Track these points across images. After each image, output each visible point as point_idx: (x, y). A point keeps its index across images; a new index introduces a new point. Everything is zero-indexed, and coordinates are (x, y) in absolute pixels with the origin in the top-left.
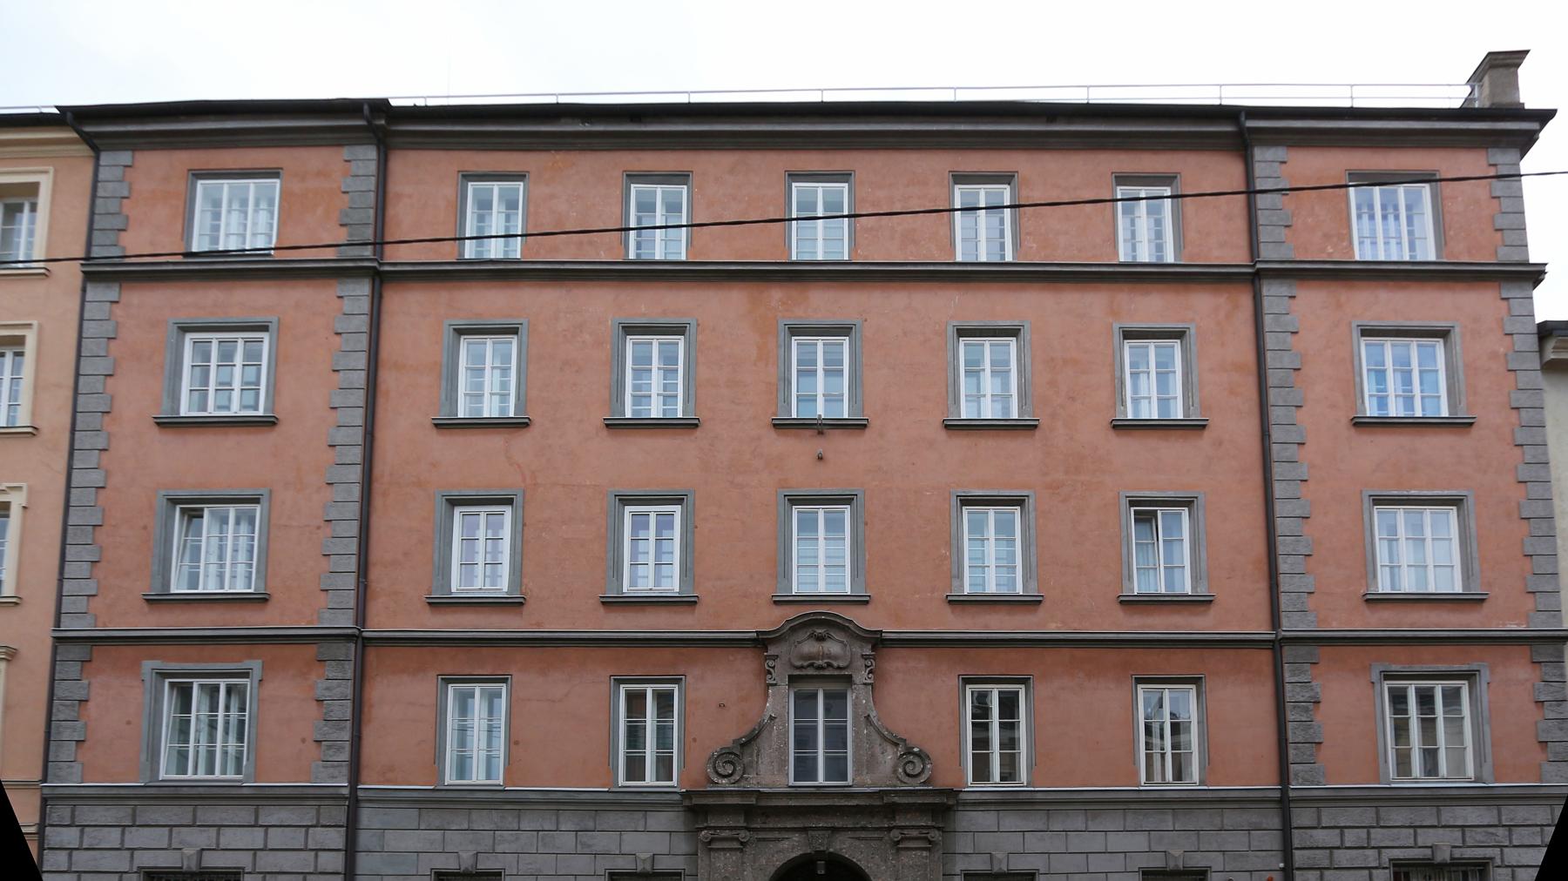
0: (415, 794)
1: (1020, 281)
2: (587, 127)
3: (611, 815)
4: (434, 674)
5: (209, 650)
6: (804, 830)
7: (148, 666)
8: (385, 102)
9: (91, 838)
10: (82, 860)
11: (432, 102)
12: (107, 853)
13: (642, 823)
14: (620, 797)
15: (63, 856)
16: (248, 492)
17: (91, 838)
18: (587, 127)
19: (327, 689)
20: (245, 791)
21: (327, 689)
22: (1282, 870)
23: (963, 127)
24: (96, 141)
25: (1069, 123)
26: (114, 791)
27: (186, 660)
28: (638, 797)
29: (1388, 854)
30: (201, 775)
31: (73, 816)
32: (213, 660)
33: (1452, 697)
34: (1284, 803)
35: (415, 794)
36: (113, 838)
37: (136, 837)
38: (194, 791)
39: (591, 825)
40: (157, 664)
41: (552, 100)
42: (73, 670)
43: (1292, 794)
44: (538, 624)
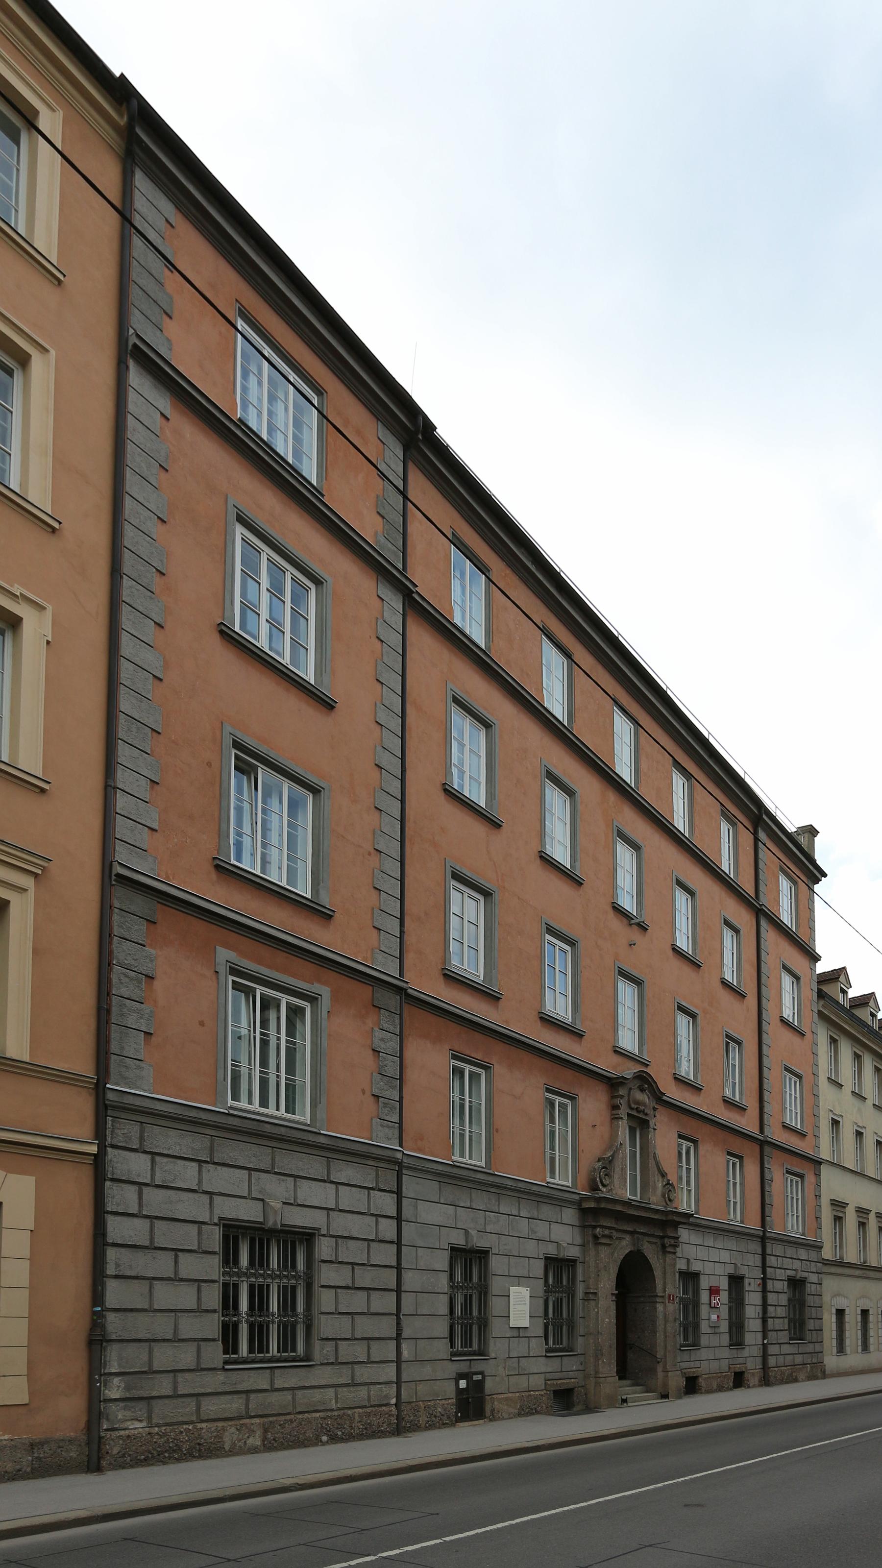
0: (440, 1168)
1: (783, 934)
2: (533, 568)
3: (172, 1133)
4: (447, 1047)
5: (281, 957)
6: (632, 1233)
7: (224, 955)
8: (434, 428)
9: (166, 1170)
10: (156, 1201)
11: (748, 780)
12: (185, 1196)
13: (536, 1213)
14: (455, 1171)
15: (131, 1193)
16: (313, 779)
17: (166, 1170)
18: (533, 568)
19: (382, 1040)
20: (322, 1140)
21: (382, 1040)
22: (762, 1279)
23: (675, 723)
24: (137, 150)
25: (715, 764)
26: (193, 1114)
27: (260, 962)
28: (471, 1174)
29: (789, 1273)
30: (256, 1106)
31: (142, 1139)
32: (285, 971)
33: (295, 1013)
34: (763, 1239)
35: (440, 1168)
36: (188, 1174)
37: (218, 1179)
38: (276, 1130)
39: (535, 1215)
40: (232, 956)
41: (706, 734)
42: (138, 929)
43: (768, 1234)
44: (507, 1022)
